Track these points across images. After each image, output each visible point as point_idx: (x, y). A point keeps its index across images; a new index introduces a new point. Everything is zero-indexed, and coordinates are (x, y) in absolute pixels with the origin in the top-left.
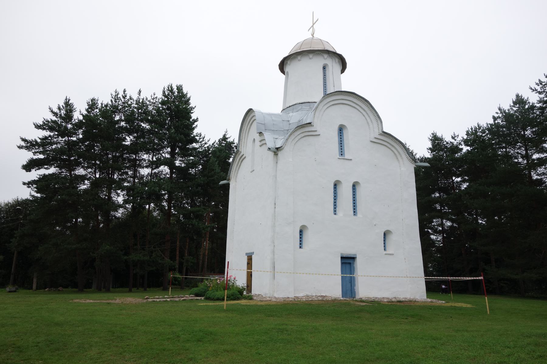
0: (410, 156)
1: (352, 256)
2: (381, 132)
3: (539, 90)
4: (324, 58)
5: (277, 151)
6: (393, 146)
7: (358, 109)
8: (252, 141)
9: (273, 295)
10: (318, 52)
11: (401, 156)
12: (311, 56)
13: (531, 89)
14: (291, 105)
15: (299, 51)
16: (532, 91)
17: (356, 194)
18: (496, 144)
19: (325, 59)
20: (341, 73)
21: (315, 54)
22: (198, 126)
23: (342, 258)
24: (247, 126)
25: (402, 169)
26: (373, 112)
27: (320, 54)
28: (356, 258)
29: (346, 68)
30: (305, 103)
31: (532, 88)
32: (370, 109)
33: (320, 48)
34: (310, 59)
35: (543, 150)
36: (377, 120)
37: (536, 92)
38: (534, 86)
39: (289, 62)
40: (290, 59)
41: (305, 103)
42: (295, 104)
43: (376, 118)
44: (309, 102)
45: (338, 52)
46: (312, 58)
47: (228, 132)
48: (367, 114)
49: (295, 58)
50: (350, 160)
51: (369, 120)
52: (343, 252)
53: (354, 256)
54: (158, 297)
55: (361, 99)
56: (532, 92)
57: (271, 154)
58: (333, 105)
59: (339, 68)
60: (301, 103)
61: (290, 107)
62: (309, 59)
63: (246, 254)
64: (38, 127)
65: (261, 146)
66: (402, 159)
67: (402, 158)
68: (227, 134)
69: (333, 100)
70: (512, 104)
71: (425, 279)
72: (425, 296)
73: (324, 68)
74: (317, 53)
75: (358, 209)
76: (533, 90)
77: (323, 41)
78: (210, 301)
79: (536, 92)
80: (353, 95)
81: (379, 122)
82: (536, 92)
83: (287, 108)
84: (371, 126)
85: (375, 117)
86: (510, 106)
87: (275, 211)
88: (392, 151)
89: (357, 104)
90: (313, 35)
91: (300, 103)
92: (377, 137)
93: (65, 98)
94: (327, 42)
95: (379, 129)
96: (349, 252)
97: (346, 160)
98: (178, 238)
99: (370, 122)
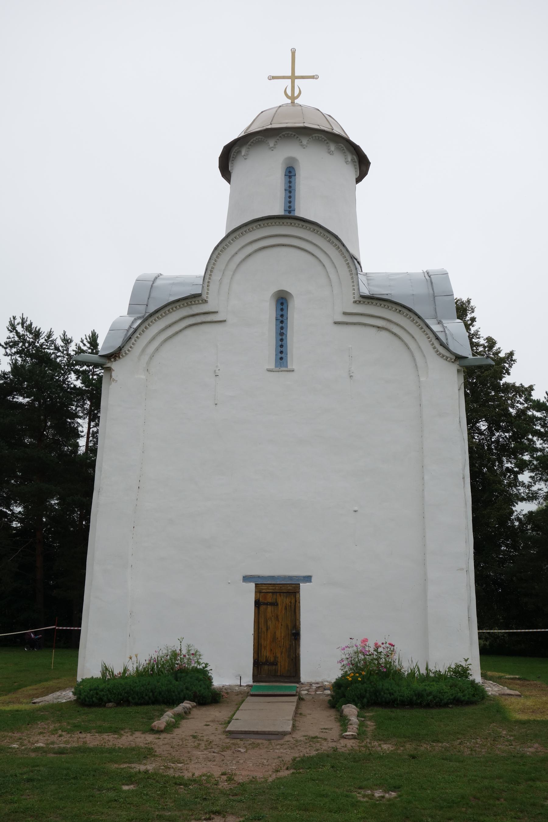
4: (302, 145)
15: (269, 127)
18: (63, 370)
21: (280, 137)
23: (244, 577)
27: (325, 140)
33: (325, 127)
39: (243, 151)
49: (259, 143)
50: (292, 372)
59: (351, 173)
64: (98, 334)
69: (243, 247)
74: (284, 135)
77: (324, 114)
90: (293, 98)
96: (313, 579)
97: (286, 373)
98: (71, 739)
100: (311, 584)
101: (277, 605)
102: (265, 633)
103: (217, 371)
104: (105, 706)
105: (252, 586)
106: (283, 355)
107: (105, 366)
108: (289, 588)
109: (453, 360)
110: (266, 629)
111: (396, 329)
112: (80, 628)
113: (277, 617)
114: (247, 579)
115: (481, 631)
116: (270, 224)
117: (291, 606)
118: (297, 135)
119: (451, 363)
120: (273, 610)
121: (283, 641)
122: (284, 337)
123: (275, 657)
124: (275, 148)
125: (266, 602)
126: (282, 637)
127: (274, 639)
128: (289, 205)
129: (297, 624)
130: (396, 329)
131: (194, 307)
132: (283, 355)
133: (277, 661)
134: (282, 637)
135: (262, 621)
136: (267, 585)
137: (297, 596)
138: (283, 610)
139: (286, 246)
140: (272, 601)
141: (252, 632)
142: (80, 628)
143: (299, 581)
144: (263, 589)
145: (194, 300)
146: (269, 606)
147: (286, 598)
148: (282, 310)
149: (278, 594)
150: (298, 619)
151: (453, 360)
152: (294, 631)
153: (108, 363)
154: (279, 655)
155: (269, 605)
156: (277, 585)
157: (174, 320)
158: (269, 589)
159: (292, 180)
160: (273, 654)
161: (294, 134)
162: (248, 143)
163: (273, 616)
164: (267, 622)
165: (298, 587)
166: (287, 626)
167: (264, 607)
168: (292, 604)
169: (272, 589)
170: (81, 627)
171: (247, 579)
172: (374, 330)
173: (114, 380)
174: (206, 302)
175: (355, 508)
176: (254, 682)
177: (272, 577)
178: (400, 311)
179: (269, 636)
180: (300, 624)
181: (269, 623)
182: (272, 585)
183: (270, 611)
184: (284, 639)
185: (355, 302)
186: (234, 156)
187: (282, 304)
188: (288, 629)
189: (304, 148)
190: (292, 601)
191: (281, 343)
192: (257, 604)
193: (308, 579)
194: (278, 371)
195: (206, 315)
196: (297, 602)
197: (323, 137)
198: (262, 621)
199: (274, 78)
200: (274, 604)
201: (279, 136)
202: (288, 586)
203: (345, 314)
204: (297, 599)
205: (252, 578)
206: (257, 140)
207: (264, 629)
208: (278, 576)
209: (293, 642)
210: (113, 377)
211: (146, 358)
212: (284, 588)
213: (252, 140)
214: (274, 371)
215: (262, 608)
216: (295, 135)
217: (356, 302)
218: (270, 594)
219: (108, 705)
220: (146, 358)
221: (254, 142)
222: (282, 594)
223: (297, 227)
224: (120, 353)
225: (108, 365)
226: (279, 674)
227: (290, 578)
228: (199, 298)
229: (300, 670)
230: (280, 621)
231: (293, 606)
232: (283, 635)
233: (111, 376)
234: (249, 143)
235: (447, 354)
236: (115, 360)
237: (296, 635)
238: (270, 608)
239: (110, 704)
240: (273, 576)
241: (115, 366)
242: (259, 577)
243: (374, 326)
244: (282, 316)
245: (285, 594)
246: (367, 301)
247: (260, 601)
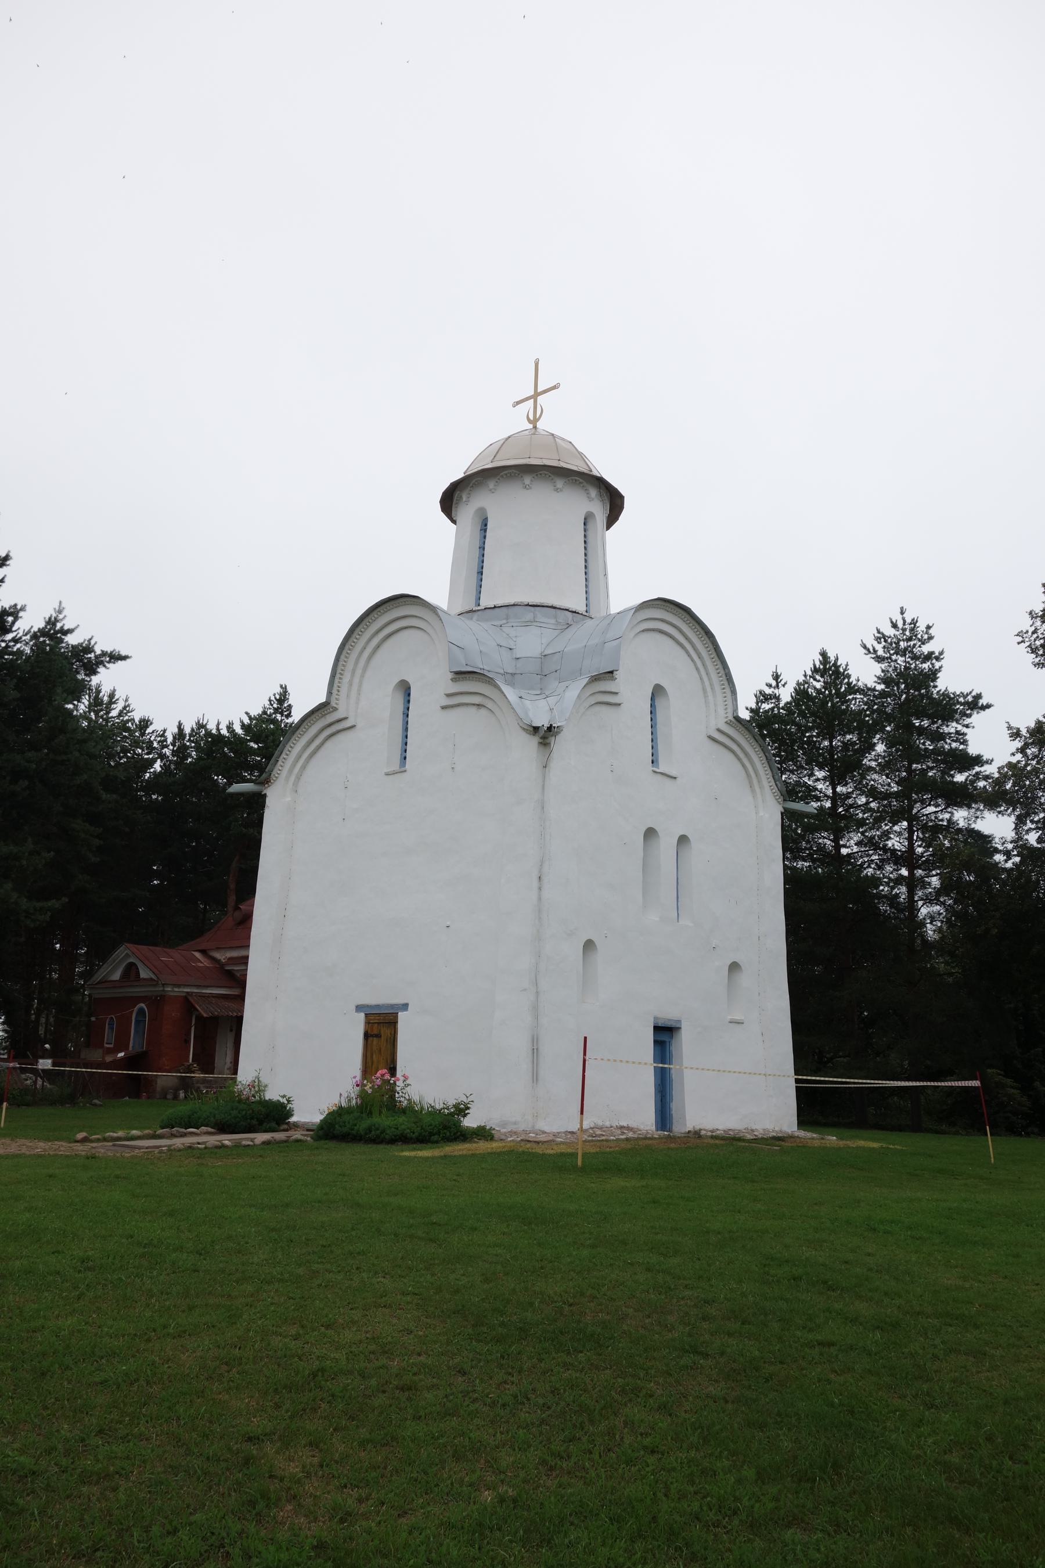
0: (779, 785)
1: (669, 1024)
2: (731, 718)
3: (880, 652)
4: (588, 497)
5: (545, 735)
6: (746, 754)
7: (687, 652)
8: (394, 684)
9: (533, 1127)
10: (546, 473)
12: (560, 483)
13: (865, 647)
14: (499, 603)
16: (867, 652)
19: (590, 499)
20: (608, 528)
22: (6, 580)
23: (657, 1029)
24: (370, 640)
25: (761, 814)
26: (716, 665)
28: (680, 1028)
30: (543, 606)
31: (867, 646)
32: (711, 654)
34: (557, 490)
35: (685, 1565)
36: (723, 685)
37: (875, 656)
38: (871, 642)
41: (543, 606)
42: (514, 605)
43: (722, 681)
44: (555, 608)
46: (561, 490)
47: (64, 613)
48: (704, 665)
51: (707, 683)
52: (660, 1015)
53: (674, 1025)
54: (121, 1134)
55: (697, 627)
56: (866, 654)
57: (534, 741)
60: (531, 606)
61: (495, 607)
62: (555, 490)
63: (655, 1018)
65: (443, 708)
66: (760, 788)
67: (761, 787)
68: (61, 616)
70: (809, 673)
71: (797, 1081)
72: (795, 1128)
76: (868, 650)
78: (405, 1146)
79: (873, 656)
80: (685, 614)
81: (728, 691)
82: (873, 656)
83: (485, 609)
85: (721, 677)
86: (805, 676)
87: (540, 899)
88: (744, 766)
89: (687, 638)
90: (534, 422)
91: (528, 605)
92: (722, 729)
93: (890, 624)
96: (668, 1014)
99: (709, 689)
100: (684, 1026)
101: (381, 1037)
105: (362, 1015)
114: (359, 1008)
115: (798, 1085)
124: (468, 501)
135: (369, 1054)
144: (371, 1020)
152: (392, 1066)
165: (395, 1016)
167: (371, 1038)
169: (378, 1020)
171: (359, 1008)
172: (474, 709)
174: (336, 709)
176: (804, 1119)
177: (378, 1006)
181: (374, 1056)
192: (366, 1036)
193: (405, 1007)
197: (515, 471)
198: (369, 1054)
200: (378, 1036)
202: (390, 1015)
203: (448, 695)
207: (370, 1064)
211: (293, 778)
218: (376, 1025)
220: (293, 778)
234: (471, 485)
242: (368, 1006)
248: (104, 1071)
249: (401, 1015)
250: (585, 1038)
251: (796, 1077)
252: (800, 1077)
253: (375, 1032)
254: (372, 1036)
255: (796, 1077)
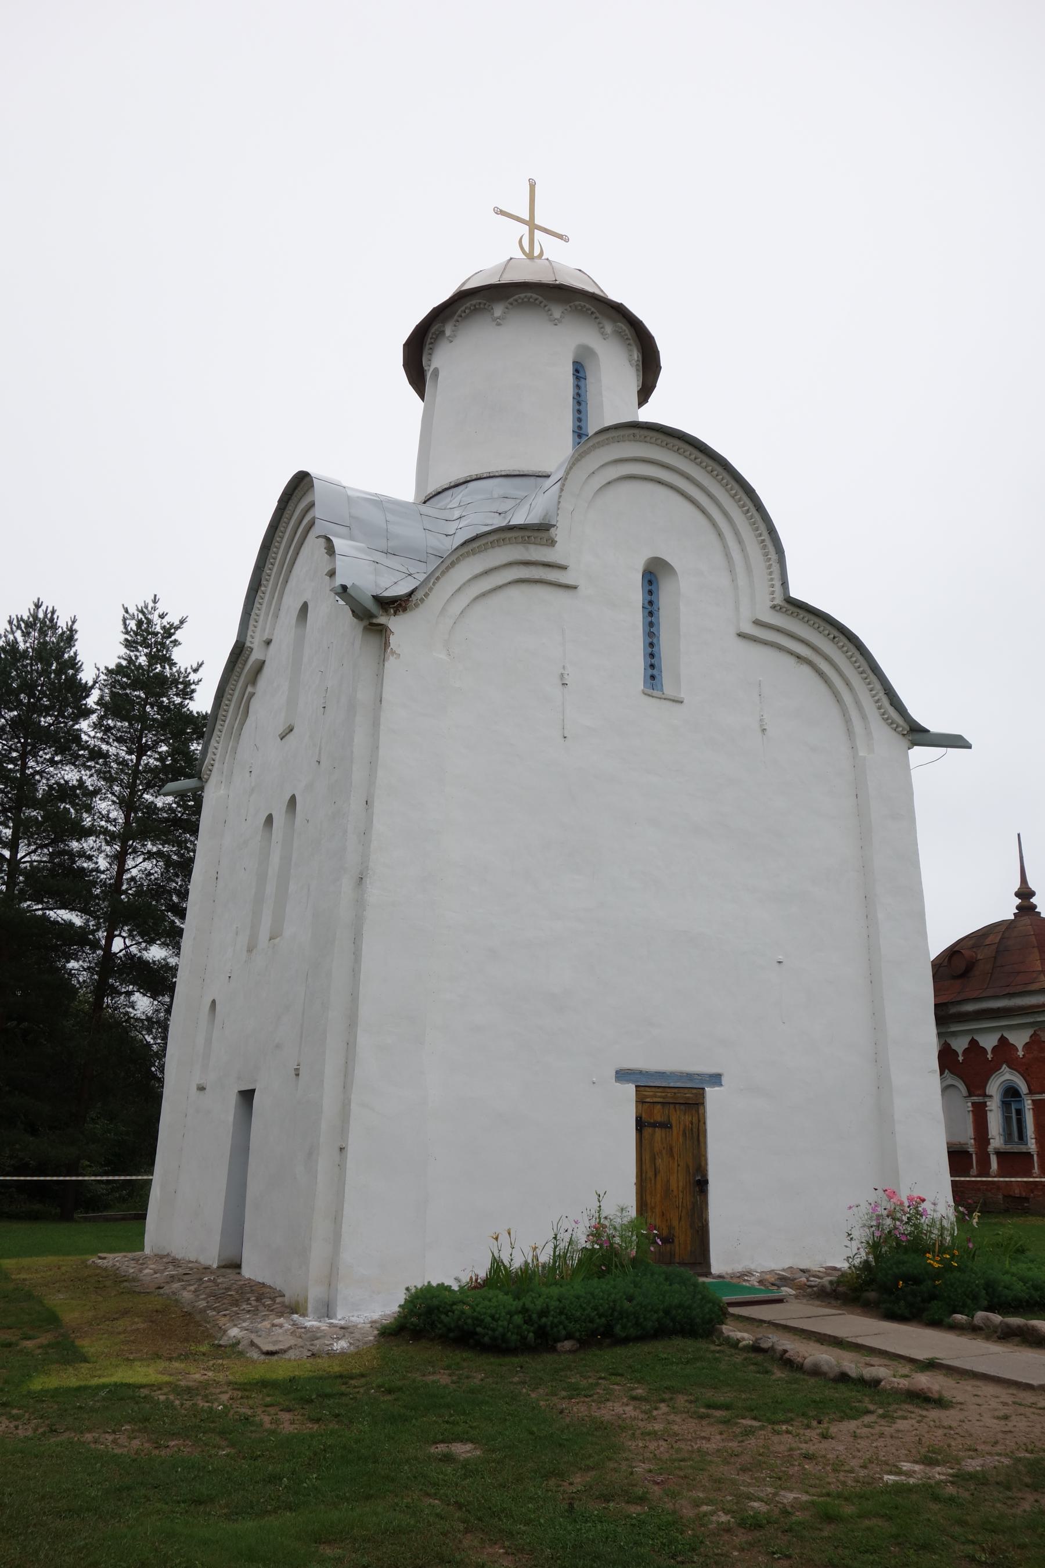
2: (779, 600)
4: (602, 334)
11: (864, 717)
17: (659, 624)
20: (639, 408)
21: (511, 304)
23: (617, 1072)
29: (404, 365)
40: (456, 317)
45: (614, 295)
58: (484, 595)
59: (632, 382)
69: (486, 573)
73: (579, 372)
74: (576, 307)
75: (663, 613)
84: (742, 580)
94: (580, 270)
95: (771, 573)
96: (724, 1080)
101: (671, 1127)
102: (653, 1181)
103: (566, 676)
104: (553, 1349)
105: (630, 1089)
106: (655, 672)
107: (375, 621)
108: (687, 1095)
109: (905, 732)
110: (653, 1173)
111: (824, 666)
112: (150, 1177)
113: (671, 1149)
114: (623, 1075)
116: (648, 439)
117: (692, 1130)
118: (598, 315)
119: (901, 736)
120: (664, 1136)
121: (681, 1196)
122: (655, 641)
123: (670, 1228)
125: (652, 1121)
126: (680, 1188)
127: (667, 1191)
128: (579, 424)
129: (703, 1164)
130: (824, 666)
131: (532, 547)
132: (655, 672)
133: (674, 1236)
134: (680, 1188)
136: (653, 1089)
137: (700, 1112)
138: (681, 1137)
139: (663, 484)
140: (662, 1120)
141: (633, 1180)
142: (150, 1177)
143: (702, 1083)
144: (647, 1097)
145: (536, 534)
146: (657, 1129)
147: (685, 1114)
148: (650, 592)
149: (672, 1106)
150: (703, 1153)
151: (905, 732)
152: (699, 1178)
153: (382, 615)
154: (675, 1223)
155: (657, 1127)
156: (668, 1090)
157: (497, 563)
158: (656, 1097)
159: (582, 383)
160: (667, 1220)
161: (593, 309)
162: (508, 298)
163: (664, 1148)
164: (655, 1159)
166: (688, 1167)
168: (694, 1125)
169: (660, 1097)
170: (152, 1175)
171: (623, 1075)
172: (791, 661)
173: (393, 652)
175: (780, 957)
177: (661, 1075)
178: (834, 638)
179: (659, 1186)
180: (706, 1164)
181: (659, 1161)
182: (660, 1090)
183: (659, 1139)
184: (683, 1192)
185: (774, 607)
186: (463, 315)
187: (650, 582)
188: (690, 1173)
189: (604, 339)
190: (694, 1121)
191: (651, 650)
192: (641, 1124)
193: (716, 1079)
194: (660, 698)
195: (547, 570)
196: (701, 1123)
198: (647, 1157)
199: (502, 213)
200: (666, 1126)
201: (457, 314)
202: (686, 1091)
203: (758, 623)
204: (701, 1116)
205: (630, 1074)
206: (526, 300)
207: (650, 1174)
208: (671, 1073)
209: (698, 1197)
210: (391, 646)
212: (679, 1095)
213: (516, 297)
214: (653, 697)
215: (647, 1131)
216: (592, 313)
217: (775, 607)
218: (659, 1106)
219: (563, 1346)
221: (520, 301)
222: (677, 1106)
223: (686, 457)
224: (408, 600)
225: (382, 620)
226: (677, 1260)
227: (690, 1076)
228: (544, 535)
229: (709, 1251)
230: (676, 1159)
231: (695, 1130)
232: (681, 1184)
233: (387, 644)
234: (511, 300)
235: (900, 720)
236: (395, 614)
237: (701, 1185)
238: (659, 1133)
239: (568, 1345)
240: (664, 1073)
241: (396, 624)
242: (641, 1072)
243: (792, 654)
244: (651, 603)
245: (682, 1107)
246: (792, 609)
247: (643, 1118)
248: (48, 1178)
249: (711, 1092)
250: (1019, 835)
251: (953, 1179)
252: (957, 1179)
253: (658, 1118)
254: (654, 1125)
255: (953, 1179)
